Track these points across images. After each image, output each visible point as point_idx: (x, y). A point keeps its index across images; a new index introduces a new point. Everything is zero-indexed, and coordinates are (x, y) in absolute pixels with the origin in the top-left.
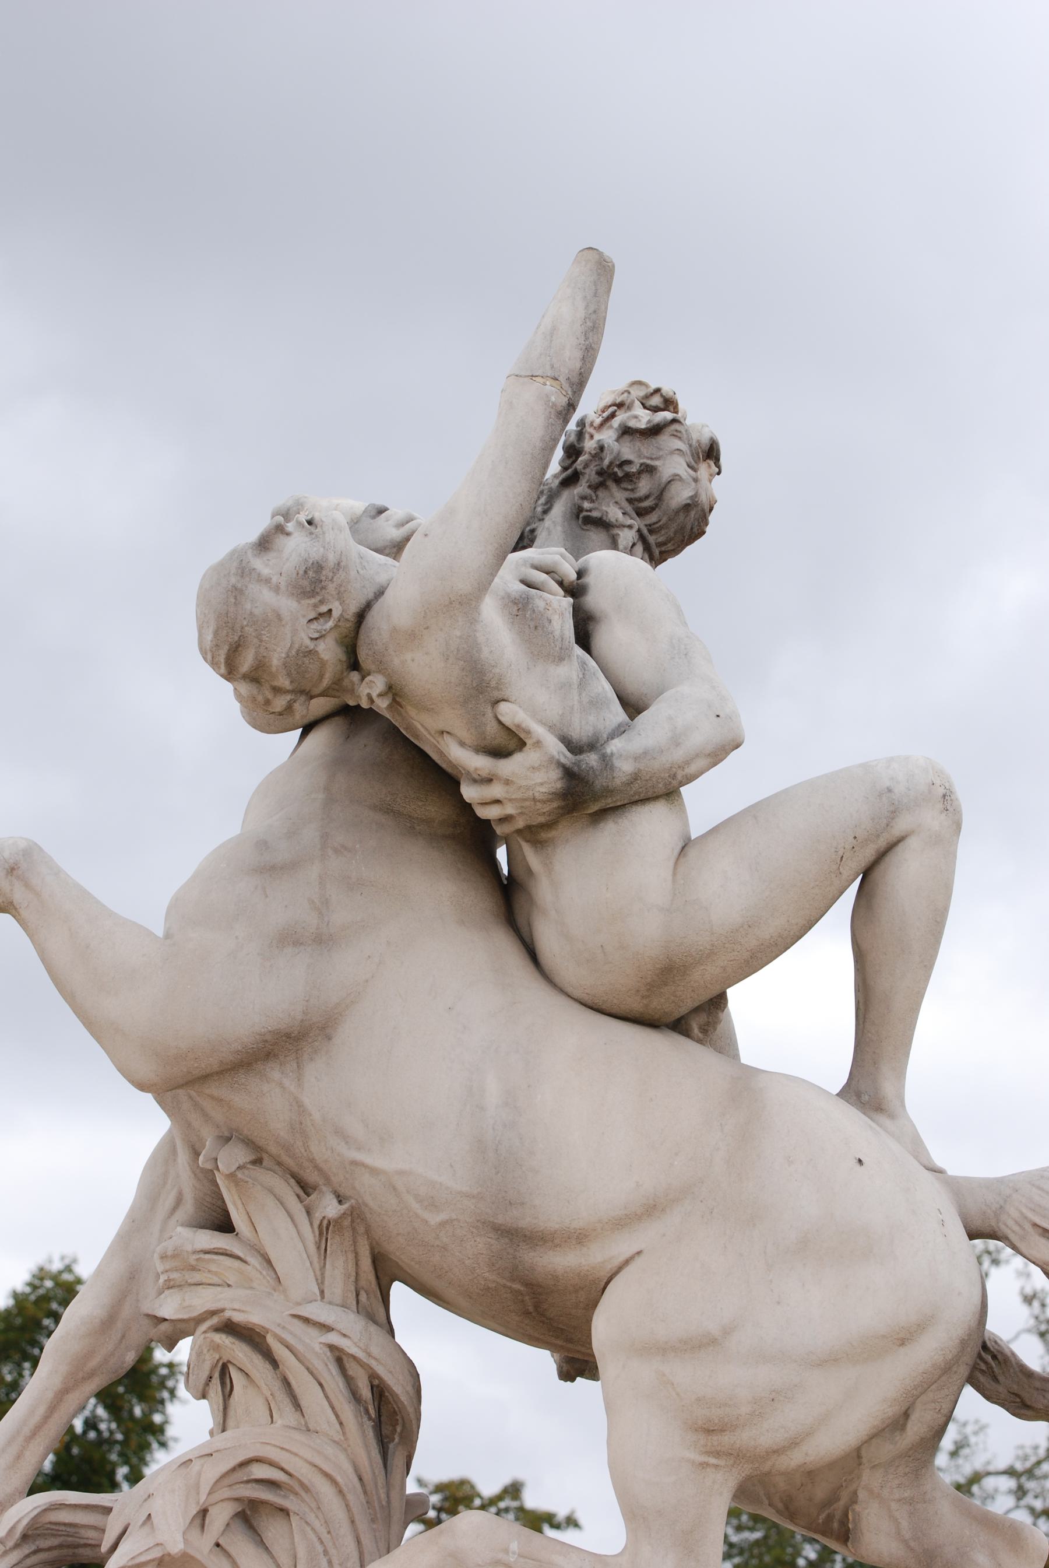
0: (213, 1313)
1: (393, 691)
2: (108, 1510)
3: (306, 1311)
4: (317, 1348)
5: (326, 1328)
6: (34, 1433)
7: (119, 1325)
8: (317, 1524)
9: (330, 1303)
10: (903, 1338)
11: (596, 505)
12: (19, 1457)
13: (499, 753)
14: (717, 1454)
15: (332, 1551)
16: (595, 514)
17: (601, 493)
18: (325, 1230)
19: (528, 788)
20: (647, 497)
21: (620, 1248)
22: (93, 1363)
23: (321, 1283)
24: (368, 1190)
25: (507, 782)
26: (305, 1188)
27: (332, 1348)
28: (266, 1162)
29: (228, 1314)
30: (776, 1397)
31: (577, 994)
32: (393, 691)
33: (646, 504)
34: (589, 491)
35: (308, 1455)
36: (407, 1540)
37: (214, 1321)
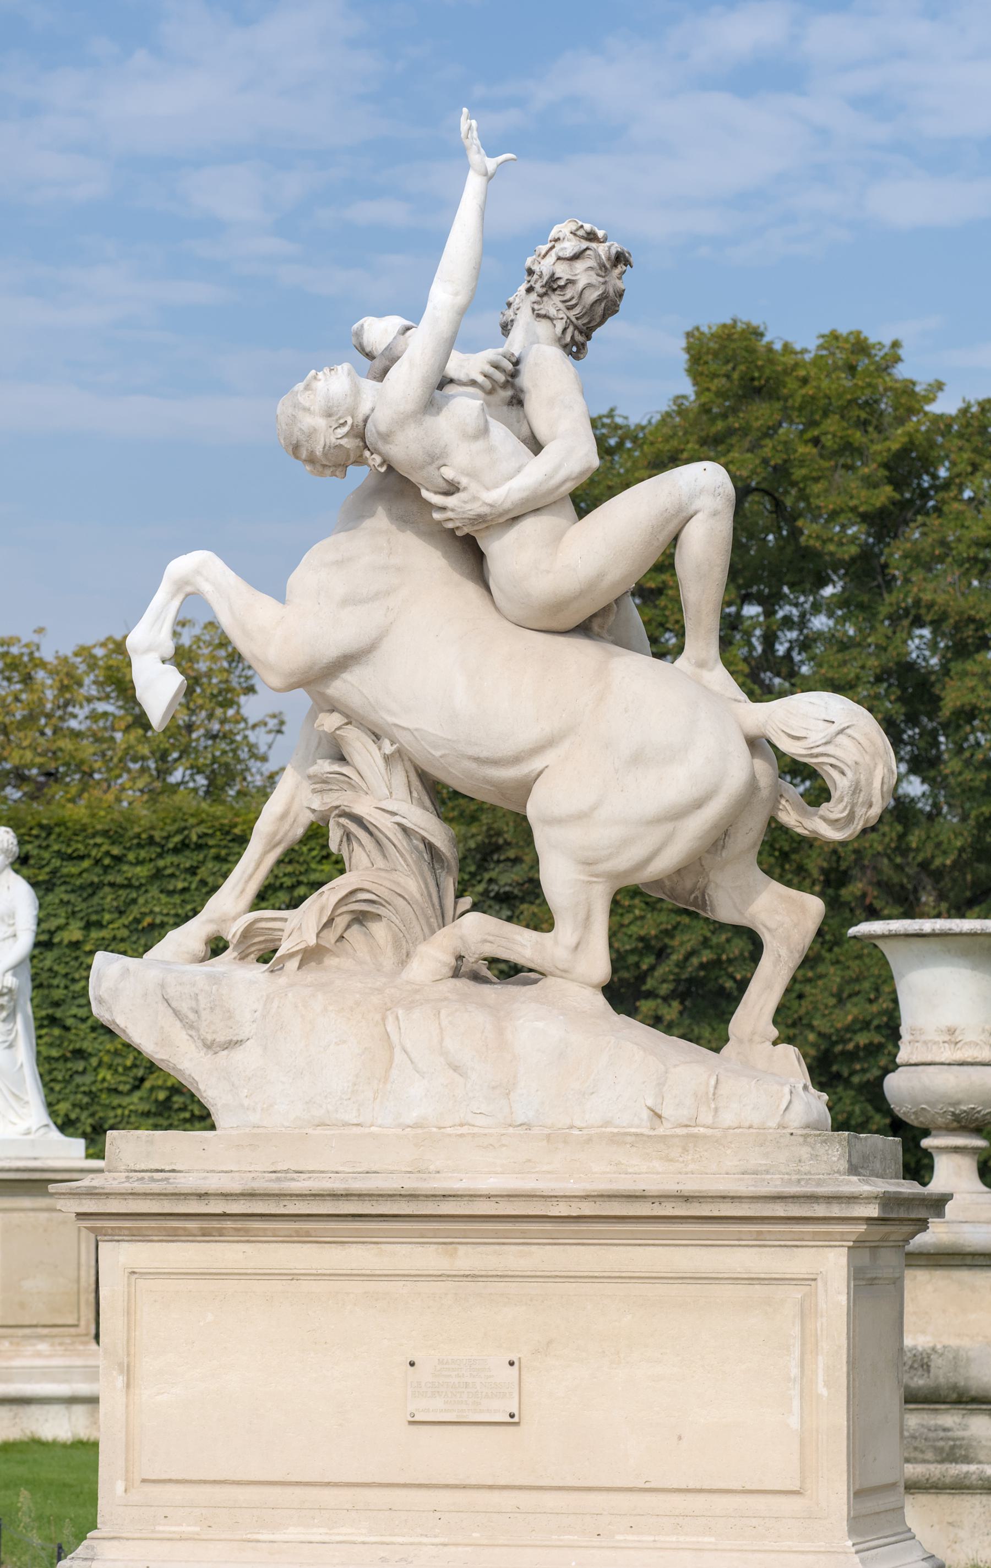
0: (337, 807)
1: (103, 645)
2: (286, 920)
3: (384, 805)
4: (390, 825)
5: (393, 814)
6: (251, 877)
7: (292, 815)
8: (397, 922)
9: (396, 799)
10: (698, 804)
11: (542, 306)
12: (242, 891)
13: (447, 493)
14: (597, 876)
15: (408, 936)
16: (543, 312)
17: (545, 299)
18: (387, 759)
19: (464, 512)
20: (572, 298)
21: (536, 764)
22: (278, 838)
23: (389, 788)
24: (405, 739)
25: (453, 510)
26: (377, 737)
27: (399, 824)
28: (354, 722)
29: (343, 807)
30: (625, 843)
31: (513, 619)
32: (103, 645)
33: (573, 302)
34: (539, 299)
35: (388, 884)
36: (280, 957)
37: (337, 812)
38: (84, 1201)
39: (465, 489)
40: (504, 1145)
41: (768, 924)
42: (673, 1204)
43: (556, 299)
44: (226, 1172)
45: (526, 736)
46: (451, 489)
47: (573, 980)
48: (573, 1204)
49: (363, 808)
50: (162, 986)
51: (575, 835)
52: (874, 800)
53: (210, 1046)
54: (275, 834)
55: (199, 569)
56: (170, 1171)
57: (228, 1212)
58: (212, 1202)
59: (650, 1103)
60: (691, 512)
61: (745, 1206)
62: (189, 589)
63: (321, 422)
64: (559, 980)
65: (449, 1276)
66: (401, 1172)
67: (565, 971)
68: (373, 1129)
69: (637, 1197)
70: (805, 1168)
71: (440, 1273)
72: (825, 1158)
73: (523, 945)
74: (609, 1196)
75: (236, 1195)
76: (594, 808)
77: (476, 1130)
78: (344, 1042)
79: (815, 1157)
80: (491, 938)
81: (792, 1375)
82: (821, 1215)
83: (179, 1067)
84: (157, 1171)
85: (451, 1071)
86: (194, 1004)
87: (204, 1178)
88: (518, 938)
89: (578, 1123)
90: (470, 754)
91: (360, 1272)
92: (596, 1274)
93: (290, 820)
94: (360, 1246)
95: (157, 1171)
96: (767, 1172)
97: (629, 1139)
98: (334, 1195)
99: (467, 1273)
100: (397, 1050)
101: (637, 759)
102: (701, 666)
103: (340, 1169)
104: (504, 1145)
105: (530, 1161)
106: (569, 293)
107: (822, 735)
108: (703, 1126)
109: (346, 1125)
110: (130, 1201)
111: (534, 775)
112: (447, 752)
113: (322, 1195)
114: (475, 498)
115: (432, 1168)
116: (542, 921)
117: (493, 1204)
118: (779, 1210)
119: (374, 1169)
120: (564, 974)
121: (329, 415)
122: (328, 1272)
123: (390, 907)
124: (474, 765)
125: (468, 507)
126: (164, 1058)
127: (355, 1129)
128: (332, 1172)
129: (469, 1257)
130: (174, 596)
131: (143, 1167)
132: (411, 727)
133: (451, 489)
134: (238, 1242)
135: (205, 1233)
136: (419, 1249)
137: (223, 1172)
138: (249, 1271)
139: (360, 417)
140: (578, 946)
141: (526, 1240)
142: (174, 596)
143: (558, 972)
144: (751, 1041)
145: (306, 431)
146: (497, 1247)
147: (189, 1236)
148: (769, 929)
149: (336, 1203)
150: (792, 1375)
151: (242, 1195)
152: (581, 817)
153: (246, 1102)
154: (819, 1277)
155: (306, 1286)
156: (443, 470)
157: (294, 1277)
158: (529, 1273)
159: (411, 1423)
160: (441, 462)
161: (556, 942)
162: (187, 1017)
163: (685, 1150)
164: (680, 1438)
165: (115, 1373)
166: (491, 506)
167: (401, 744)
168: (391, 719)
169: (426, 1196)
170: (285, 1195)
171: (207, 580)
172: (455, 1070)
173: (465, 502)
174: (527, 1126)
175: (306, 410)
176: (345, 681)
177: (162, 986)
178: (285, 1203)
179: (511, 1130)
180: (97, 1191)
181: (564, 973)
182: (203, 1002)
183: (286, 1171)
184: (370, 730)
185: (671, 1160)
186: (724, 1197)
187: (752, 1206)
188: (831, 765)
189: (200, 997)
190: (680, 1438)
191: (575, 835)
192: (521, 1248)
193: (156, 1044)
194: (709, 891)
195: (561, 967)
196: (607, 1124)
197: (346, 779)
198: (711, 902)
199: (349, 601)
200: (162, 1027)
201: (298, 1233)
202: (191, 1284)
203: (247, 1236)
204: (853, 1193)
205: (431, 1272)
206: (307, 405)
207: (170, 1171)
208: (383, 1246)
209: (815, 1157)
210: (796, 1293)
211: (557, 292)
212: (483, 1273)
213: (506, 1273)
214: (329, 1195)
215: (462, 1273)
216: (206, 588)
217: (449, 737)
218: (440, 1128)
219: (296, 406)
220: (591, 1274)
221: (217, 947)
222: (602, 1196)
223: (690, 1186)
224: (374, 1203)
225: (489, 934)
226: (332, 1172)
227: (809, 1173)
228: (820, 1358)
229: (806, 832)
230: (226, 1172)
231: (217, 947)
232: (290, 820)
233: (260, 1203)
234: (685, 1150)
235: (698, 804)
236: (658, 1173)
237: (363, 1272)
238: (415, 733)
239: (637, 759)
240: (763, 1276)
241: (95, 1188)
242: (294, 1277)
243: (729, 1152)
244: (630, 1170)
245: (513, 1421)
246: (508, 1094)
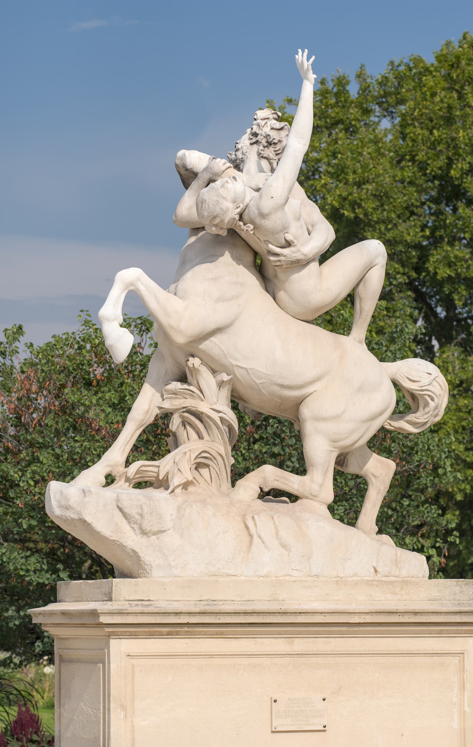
3: (215, 407)
5: (219, 412)
7: (151, 410)
8: (216, 469)
10: (381, 414)
12: (124, 450)
14: (335, 448)
16: (265, 155)
17: (266, 148)
21: (310, 389)
22: (144, 422)
23: (218, 398)
25: (285, 256)
38: (114, 617)
39: (295, 245)
40: (315, 586)
41: (376, 474)
42: (409, 616)
43: (272, 149)
44: (176, 601)
45: (310, 374)
46: (288, 244)
47: (317, 501)
48: (361, 617)
49: (203, 407)
50: (118, 500)
51: (331, 427)
52: (440, 413)
53: (144, 533)
54: (143, 420)
55: (131, 276)
56: (147, 601)
57: (190, 622)
58: (182, 617)
59: (374, 565)
60: (374, 264)
61: (442, 617)
62: (132, 288)
63: (230, 205)
64: (310, 501)
65: (289, 654)
66: (265, 600)
67: (315, 496)
68: (242, 577)
69: (393, 613)
70: (457, 598)
71: (286, 653)
72: (466, 592)
73: (293, 482)
74: (380, 612)
75: (196, 613)
76: (343, 413)
77: (296, 579)
78: (227, 532)
79: (462, 592)
80: (278, 479)
81: (454, 701)
82: (357, 621)
83: (124, 544)
84: (141, 600)
85: (281, 548)
86: (139, 511)
87: (170, 604)
88: (291, 478)
89: (341, 575)
90: (279, 382)
91: (245, 653)
92: (362, 652)
93: (150, 413)
94: (245, 639)
95: (141, 600)
96: (440, 600)
97: (375, 583)
98: (246, 613)
99: (299, 653)
100: (255, 537)
101: (361, 389)
102: (354, 345)
103: (235, 599)
104: (315, 586)
105: (328, 594)
106: (278, 147)
107: (428, 380)
108: (394, 576)
109: (228, 575)
110: (139, 617)
111: (307, 395)
112: (265, 381)
113: (240, 613)
114: (299, 251)
115: (280, 598)
116: (301, 470)
117: (323, 617)
118: (458, 619)
119: (252, 599)
120: (314, 498)
121: (234, 202)
122: (229, 653)
123: (215, 461)
124: (277, 389)
125: (294, 255)
126: (116, 539)
127: (233, 577)
128: (231, 601)
129: (301, 644)
130: (123, 291)
131: (133, 599)
132: (247, 367)
133: (288, 244)
134: (183, 638)
135: (169, 634)
136: (275, 640)
137: (175, 601)
138: (189, 654)
139: (245, 204)
140: (319, 484)
141: (329, 634)
142: (123, 291)
143: (311, 497)
144: (370, 532)
145: (224, 209)
146: (313, 639)
147: (160, 635)
148: (375, 476)
149: (245, 617)
150: (454, 701)
151: (199, 613)
152: (336, 418)
153: (172, 563)
154: (465, 652)
155: (217, 661)
156: (286, 235)
157: (211, 656)
158: (329, 653)
159: (273, 732)
160: (286, 231)
161: (312, 481)
162: (134, 518)
163: (402, 588)
164: (402, 735)
165: (119, 710)
166: (305, 255)
167: (235, 375)
168: (235, 363)
169: (291, 613)
170: (221, 613)
171: (142, 284)
172: (283, 547)
173: (293, 252)
174: (317, 576)
175: (225, 198)
176: (211, 341)
177: (118, 500)
178: (219, 617)
179: (309, 578)
180: (124, 612)
181: (313, 497)
182: (146, 510)
183: (207, 600)
184: (210, 367)
185: (396, 594)
186: (433, 613)
187: (446, 617)
188: (429, 396)
189: (143, 507)
190: (402, 735)
191: (331, 427)
192: (325, 639)
193: (112, 532)
194: (348, 457)
195: (313, 494)
196: (355, 575)
197: (191, 393)
198: (347, 462)
199: (221, 299)
200: (117, 523)
201: (217, 633)
202: (157, 662)
203: (189, 635)
204: (54, 610)
205: (281, 653)
206: (225, 195)
207: (147, 601)
208: (257, 639)
209: (462, 592)
210: (455, 660)
211: (272, 146)
212: (307, 653)
213: (318, 653)
214: (243, 613)
215: (296, 653)
216: (142, 288)
217: (270, 374)
218: (276, 577)
219: (219, 195)
220: (359, 652)
221: (110, 480)
222: (377, 612)
223: (418, 607)
224: (264, 617)
225: (278, 476)
226: (231, 601)
227: (460, 600)
228: (466, 693)
229: (393, 428)
230: (176, 601)
231: (110, 480)
232: (150, 413)
233: (207, 617)
234: (402, 588)
235: (381, 414)
236: (390, 600)
237: (248, 653)
238: (250, 371)
239: (361, 389)
240: (440, 652)
241: (123, 610)
242: (211, 656)
243: (422, 589)
244: (376, 599)
245: (324, 729)
246: (309, 560)
